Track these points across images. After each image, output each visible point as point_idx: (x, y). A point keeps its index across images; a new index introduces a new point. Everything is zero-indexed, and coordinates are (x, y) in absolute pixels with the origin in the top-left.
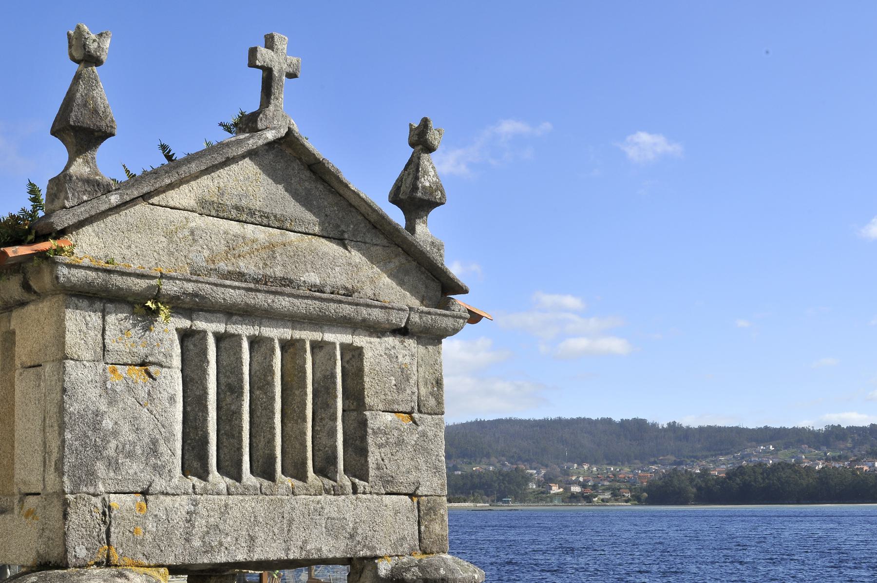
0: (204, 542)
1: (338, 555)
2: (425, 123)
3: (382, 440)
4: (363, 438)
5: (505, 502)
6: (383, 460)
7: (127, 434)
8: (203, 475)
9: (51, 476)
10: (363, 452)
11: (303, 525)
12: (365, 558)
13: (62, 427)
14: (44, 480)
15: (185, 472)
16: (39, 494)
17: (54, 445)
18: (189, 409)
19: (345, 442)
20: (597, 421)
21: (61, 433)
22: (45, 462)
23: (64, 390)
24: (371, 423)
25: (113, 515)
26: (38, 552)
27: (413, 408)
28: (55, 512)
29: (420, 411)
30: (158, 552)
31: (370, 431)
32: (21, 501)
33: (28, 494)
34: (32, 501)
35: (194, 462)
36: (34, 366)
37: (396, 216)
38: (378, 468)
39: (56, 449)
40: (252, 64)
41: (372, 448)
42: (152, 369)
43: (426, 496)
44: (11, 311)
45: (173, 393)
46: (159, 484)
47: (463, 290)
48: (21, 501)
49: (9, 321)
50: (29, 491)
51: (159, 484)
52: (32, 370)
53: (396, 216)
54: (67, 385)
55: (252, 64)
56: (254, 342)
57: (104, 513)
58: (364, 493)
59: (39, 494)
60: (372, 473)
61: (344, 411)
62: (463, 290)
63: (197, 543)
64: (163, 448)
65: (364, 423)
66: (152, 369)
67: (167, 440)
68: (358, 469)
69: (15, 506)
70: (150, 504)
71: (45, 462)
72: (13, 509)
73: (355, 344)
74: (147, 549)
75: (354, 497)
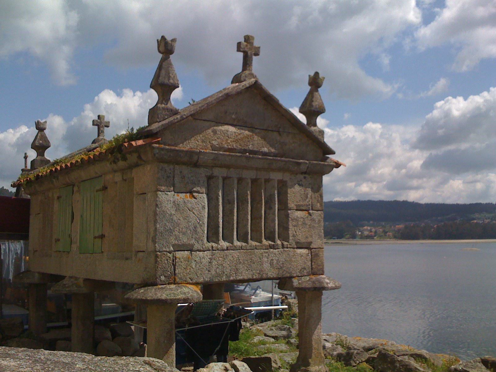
0: (216, 272)
1: (275, 276)
2: (317, 74)
3: (294, 223)
4: (287, 223)
5: (334, 239)
6: (296, 232)
7: (183, 224)
8: (217, 241)
9: (150, 244)
10: (287, 229)
11: (260, 263)
12: (287, 277)
13: (155, 222)
14: (147, 246)
15: (208, 241)
16: (144, 251)
17: (152, 230)
18: (210, 211)
19: (278, 224)
20: (377, 201)
21: (155, 225)
22: (147, 237)
23: (157, 205)
24: (290, 216)
25: (177, 261)
26: (143, 278)
27: (309, 208)
28: (152, 260)
29: (312, 210)
30: (196, 277)
31: (290, 219)
32: (136, 255)
33: (139, 251)
34: (141, 254)
35: (212, 235)
36: (142, 194)
37: (302, 118)
38: (294, 236)
39: (153, 232)
40: (239, 50)
41: (291, 227)
42: (195, 194)
43: (315, 248)
44: (132, 169)
45: (204, 205)
46: (197, 246)
47: (333, 153)
48: (136, 255)
49: (131, 174)
50: (140, 250)
51: (197, 246)
52: (141, 196)
53: (302, 118)
54: (158, 203)
55: (239, 50)
56: (240, 180)
57: (173, 261)
58: (287, 248)
59: (144, 251)
60: (291, 238)
61: (278, 210)
62: (333, 153)
63: (213, 272)
64: (199, 230)
65: (287, 216)
66: (195, 194)
67: (201, 226)
68: (284, 237)
69: (133, 256)
70: (193, 255)
71: (147, 237)
72: (132, 257)
73: (284, 180)
74: (191, 276)
75: (282, 250)
